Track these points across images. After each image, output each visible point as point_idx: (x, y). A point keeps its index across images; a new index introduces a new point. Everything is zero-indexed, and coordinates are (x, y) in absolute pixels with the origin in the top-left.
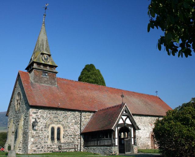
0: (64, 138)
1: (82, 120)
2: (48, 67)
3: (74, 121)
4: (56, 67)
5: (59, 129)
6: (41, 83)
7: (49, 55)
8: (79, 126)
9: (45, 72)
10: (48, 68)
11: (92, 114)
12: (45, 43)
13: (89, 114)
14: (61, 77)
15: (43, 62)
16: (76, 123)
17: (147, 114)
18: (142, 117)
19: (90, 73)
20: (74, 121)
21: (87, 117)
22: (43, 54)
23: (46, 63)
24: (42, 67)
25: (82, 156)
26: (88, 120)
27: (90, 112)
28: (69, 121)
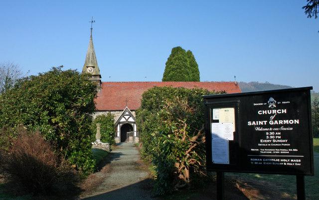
7: (94, 67)
13: (119, 112)
27: (120, 111)
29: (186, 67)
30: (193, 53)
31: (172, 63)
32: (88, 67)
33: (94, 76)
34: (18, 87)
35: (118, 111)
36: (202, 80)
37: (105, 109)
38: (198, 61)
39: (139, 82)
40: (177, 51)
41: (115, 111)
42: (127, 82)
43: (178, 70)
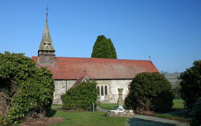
0: (55, 96)
1: (68, 85)
2: (49, 52)
3: (62, 86)
4: (54, 51)
5: (106, 87)
6: (44, 63)
7: (50, 44)
8: (65, 89)
9: (47, 55)
10: (49, 53)
11: (75, 81)
12: (47, 36)
13: (73, 81)
14: (59, 56)
15: (45, 50)
16: (63, 87)
17: (124, 78)
18: (119, 80)
19: (100, 43)
20: (62, 86)
21: (71, 83)
22: (45, 44)
23: (47, 50)
24: (45, 52)
25: (163, 113)
26: (72, 85)
27: (74, 80)
28: (58, 86)
29: (108, 49)
30: (112, 41)
31: (99, 47)
32: (45, 44)
33: (50, 51)
34: (49, 87)
35: (72, 80)
36: (119, 57)
37: (62, 79)
38: (115, 46)
39: (84, 58)
40: (101, 39)
41: (70, 80)
42: (75, 58)
43: (104, 52)
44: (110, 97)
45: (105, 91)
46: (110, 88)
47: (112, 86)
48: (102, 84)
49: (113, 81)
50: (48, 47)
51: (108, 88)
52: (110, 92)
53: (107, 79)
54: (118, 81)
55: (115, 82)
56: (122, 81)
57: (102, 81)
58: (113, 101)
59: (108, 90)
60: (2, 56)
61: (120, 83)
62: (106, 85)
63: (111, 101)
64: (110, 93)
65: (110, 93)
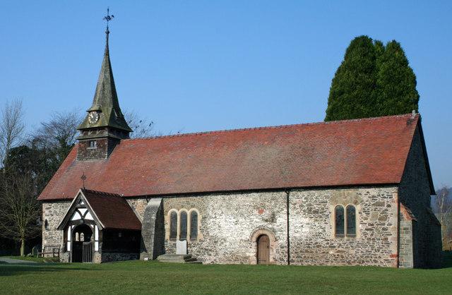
5: (194, 216)
17: (244, 187)
40: (362, 46)
44: (205, 245)
45: (189, 227)
46: (204, 218)
47: (210, 213)
48: (182, 207)
49: (214, 197)
50: (95, 118)
51: (200, 218)
52: (205, 229)
53: (196, 194)
54: (227, 197)
55: (220, 202)
56: (240, 197)
57: (183, 200)
58: (213, 258)
59: (199, 224)
60: (7, 174)
61: (235, 204)
62: (182, 210)
63: (207, 257)
64: (205, 233)
65: (205, 233)
